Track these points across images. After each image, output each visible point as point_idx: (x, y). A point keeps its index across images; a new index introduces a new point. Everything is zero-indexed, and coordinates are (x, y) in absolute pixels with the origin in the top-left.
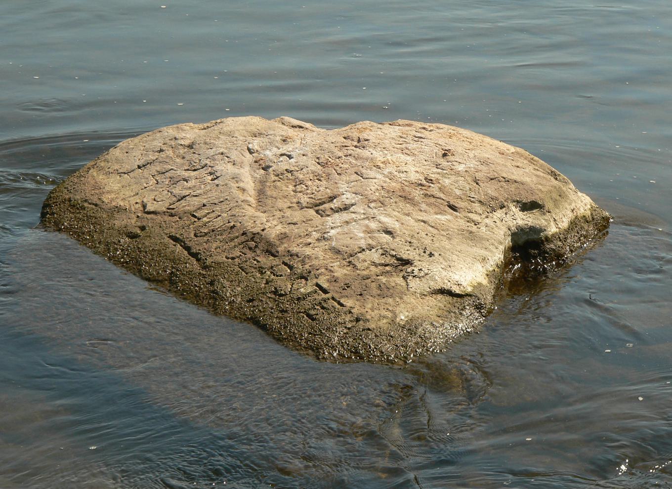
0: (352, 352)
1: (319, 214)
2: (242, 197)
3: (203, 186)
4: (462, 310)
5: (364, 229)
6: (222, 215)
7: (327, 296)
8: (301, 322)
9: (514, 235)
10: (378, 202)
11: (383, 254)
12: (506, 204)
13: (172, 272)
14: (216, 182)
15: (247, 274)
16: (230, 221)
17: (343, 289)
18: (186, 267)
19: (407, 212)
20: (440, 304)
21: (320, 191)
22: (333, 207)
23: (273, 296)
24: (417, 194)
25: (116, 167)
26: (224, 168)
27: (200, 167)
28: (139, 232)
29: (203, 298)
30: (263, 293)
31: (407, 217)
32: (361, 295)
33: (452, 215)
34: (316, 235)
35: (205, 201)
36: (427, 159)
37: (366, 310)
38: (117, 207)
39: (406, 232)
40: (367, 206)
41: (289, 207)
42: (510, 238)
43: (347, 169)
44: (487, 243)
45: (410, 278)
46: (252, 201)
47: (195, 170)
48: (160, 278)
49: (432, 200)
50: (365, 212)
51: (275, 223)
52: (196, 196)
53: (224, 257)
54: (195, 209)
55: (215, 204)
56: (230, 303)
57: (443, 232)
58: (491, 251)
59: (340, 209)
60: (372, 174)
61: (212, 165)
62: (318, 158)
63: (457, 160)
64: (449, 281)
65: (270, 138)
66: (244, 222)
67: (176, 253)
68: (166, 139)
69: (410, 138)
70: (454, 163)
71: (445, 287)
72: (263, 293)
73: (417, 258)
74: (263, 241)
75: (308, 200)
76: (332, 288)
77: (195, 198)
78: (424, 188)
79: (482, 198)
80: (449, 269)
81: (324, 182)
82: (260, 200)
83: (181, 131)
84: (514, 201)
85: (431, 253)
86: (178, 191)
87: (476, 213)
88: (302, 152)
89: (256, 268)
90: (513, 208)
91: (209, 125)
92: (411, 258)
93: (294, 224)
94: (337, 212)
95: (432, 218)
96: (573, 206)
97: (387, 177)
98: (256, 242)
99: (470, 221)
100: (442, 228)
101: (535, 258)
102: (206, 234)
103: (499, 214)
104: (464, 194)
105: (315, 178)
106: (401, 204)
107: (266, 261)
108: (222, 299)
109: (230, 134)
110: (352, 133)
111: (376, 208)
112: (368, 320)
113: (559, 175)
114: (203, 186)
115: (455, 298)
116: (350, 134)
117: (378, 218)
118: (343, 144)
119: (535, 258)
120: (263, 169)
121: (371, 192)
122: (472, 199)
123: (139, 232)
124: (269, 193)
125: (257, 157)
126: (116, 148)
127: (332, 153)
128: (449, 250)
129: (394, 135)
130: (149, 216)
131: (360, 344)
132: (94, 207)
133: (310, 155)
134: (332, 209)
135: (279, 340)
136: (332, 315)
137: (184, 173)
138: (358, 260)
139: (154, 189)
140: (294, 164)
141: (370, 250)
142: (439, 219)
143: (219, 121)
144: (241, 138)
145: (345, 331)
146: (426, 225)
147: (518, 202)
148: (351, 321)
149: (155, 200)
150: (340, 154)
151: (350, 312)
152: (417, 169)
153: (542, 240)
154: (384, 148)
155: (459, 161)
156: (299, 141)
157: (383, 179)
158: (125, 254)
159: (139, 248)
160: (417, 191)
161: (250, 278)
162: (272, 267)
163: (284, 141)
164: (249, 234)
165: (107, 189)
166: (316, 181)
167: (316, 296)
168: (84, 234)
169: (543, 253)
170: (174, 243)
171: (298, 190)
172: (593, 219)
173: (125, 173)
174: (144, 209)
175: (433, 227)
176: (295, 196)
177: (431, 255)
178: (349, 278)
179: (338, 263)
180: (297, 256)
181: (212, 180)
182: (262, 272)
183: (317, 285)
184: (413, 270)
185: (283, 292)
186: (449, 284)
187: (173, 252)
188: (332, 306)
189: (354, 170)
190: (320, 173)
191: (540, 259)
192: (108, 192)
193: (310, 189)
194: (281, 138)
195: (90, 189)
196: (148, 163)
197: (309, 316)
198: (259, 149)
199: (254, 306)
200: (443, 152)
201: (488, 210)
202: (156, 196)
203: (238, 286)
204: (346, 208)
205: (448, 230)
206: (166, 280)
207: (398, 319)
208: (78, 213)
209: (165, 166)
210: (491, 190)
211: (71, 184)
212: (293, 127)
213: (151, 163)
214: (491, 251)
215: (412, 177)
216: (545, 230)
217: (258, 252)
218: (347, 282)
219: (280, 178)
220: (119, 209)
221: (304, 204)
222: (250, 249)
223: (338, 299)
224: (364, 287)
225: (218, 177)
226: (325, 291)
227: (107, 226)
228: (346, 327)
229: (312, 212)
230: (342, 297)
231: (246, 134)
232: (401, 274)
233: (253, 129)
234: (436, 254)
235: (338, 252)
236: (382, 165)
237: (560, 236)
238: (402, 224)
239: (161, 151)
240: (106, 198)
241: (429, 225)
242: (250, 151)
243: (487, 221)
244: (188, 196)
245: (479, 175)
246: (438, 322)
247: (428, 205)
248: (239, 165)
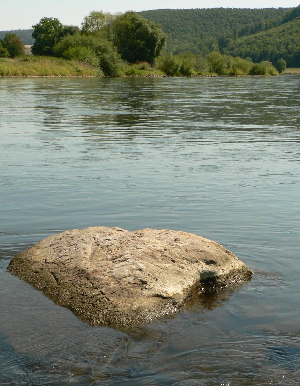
0: (107, 321)
4: (166, 304)
5: (129, 268)
7: (104, 296)
11: (135, 279)
12: (199, 261)
20: (156, 302)
24: (158, 255)
26: (82, 245)
30: (78, 295)
33: (172, 264)
34: (108, 271)
36: (167, 241)
42: (199, 276)
44: (186, 276)
46: (88, 257)
49: (165, 257)
57: (166, 271)
58: (187, 280)
60: (141, 247)
62: (120, 241)
72: (78, 295)
74: (86, 273)
76: (107, 293)
77: (66, 257)
79: (188, 258)
81: (120, 250)
84: (203, 260)
85: (157, 279)
86: (60, 254)
87: (184, 264)
88: (115, 238)
89: (79, 284)
90: (202, 263)
93: (101, 266)
94: (122, 262)
95: (163, 265)
96: (233, 264)
97: (147, 248)
99: (180, 267)
101: (212, 286)
102: (64, 271)
103: (195, 265)
107: (83, 281)
112: (119, 307)
113: (230, 253)
128: (166, 278)
133: (117, 239)
134: (119, 260)
135: (77, 315)
145: (107, 312)
147: (205, 260)
150: (130, 239)
151: (112, 303)
152: (161, 245)
162: (85, 284)
169: (215, 284)
172: (243, 271)
177: (157, 280)
178: (116, 288)
180: (97, 279)
183: (101, 292)
185: (86, 295)
186: (162, 292)
190: (119, 246)
192: (35, 255)
197: (93, 305)
198: (98, 238)
203: (69, 292)
205: (168, 270)
210: (193, 254)
212: (117, 230)
214: (187, 280)
220: (36, 262)
224: (121, 293)
226: (103, 294)
228: (107, 310)
229: (111, 262)
232: (141, 288)
234: (159, 280)
236: (146, 243)
237: (225, 277)
242: (94, 238)
243: (189, 267)
245: (188, 249)
246: (152, 309)
247: (163, 259)
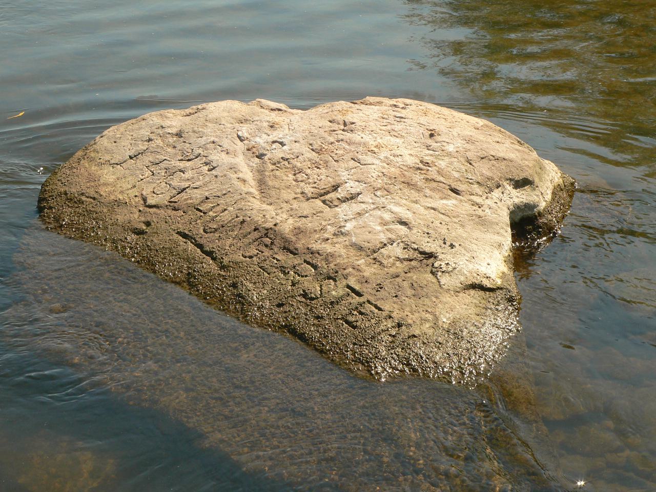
1: (327, 205)
2: (245, 189)
3: (201, 177)
5: (379, 221)
6: (228, 208)
8: (342, 331)
9: (512, 214)
10: (383, 189)
11: (404, 248)
13: (189, 274)
14: (214, 172)
15: (269, 274)
16: (239, 215)
17: (377, 291)
18: (203, 267)
19: (415, 199)
20: (475, 301)
21: (321, 179)
22: (339, 197)
23: (303, 300)
24: (417, 178)
25: (107, 157)
26: (216, 157)
27: (194, 157)
28: (144, 228)
29: (229, 302)
31: (416, 205)
32: (396, 296)
35: (207, 194)
36: (416, 140)
37: (406, 313)
38: (116, 201)
39: (420, 222)
40: (373, 195)
41: (295, 198)
43: (343, 156)
45: (440, 274)
46: (254, 191)
47: (189, 160)
48: (178, 280)
49: (434, 185)
50: (373, 201)
51: (285, 216)
52: (196, 188)
53: (241, 255)
54: (198, 202)
55: (219, 197)
56: (259, 308)
57: (454, 220)
59: (347, 198)
61: (206, 155)
62: (311, 144)
63: (444, 140)
64: (478, 275)
65: (256, 125)
66: (254, 217)
67: (189, 251)
68: (153, 128)
69: (392, 118)
70: (445, 144)
71: (476, 281)
73: (439, 250)
74: (278, 237)
75: (312, 190)
77: (195, 191)
78: (423, 172)
79: (479, 179)
80: (473, 260)
81: (323, 169)
82: (262, 191)
83: (165, 119)
84: (507, 180)
87: (477, 195)
88: (293, 139)
89: (277, 268)
91: (191, 111)
92: (433, 250)
93: (305, 217)
95: (440, 204)
97: (384, 162)
98: (270, 238)
100: (453, 215)
102: (216, 230)
103: (496, 193)
104: (462, 176)
105: (313, 166)
106: (406, 191)
108: (250, 304)
109: (217, 121)
110: (336, 116)
111: (383, 197)
114: (201, 177)
115: (488, 293)
116: (334, 117)
117: (388, 207)
118: (332, 129)
119: (530, 233)
120: (257, 157)
121: (373, 179)
122: (471, 181)
123: (144, 228)
124: (270, 183)
125: (248, 145)
126: (102, 137)
127: (324, 138)
128: (466, 239)
129: (376, 116)
130: (153, 210)
131: (410, 354)
132: (92, 200)
136: (373, 321)
137: (178, 163)
138: (383, 256)
139: (151, 181)
140: (289, 152)
141: (392, 244)
142: (446, 204)
143: (200, 107)
144: (229, 125)
146: (437, 212)
147: (511, 180)
148: (393, 327)
149: (154, 192)
150: (332, 139)
151: (390, 317)
153: (536, 216)
154: (372, 131)
155: (447, 140)
156: (286, 127)
157: (381, 164)
158: (135, 253)
159: (148, 246)
160: (417, 176)
161: (274, 279)
162: (294, 267)
163: (272, 127)
164: (261, 229)
165: (102, 181)
166: (315, 169)
167: (350, 300)
168: (87, 230)
169: (537, 228)
170: (184, 240)
171: (300, 179)
173: (117, 164)
174: (145, 203)
175: (444, 214)
176: (298, 186)
179: (363, 260)
180: (319, 253)
181: (209, 170)
182: (284, 272)
183: (348, 287)
184: (441, 265)
185: (313, 296)
186: (479, 277)
187: (185, 250)
188: (370, 311)
189: (351, 155)
191: (535, 234)
193: (311, 178)
194: (267, 123)
195: (84, 181)
196: (139, 153)
197: (347, 322)
198: (249, 136)
199: (285, 312)
200: (430, 133)
201: (487, 191)
202: (154, 188)
204: (352, 197)
205: (458, 216)
206: (184, 282)
207: (440, 322)
208: (77, 207)
209: (158, 157)
210: (484, 169)
211: (64, 176)
212: (272, 110)
213: (142, 153)
215: (408, 161)
216: (538, 205)
217: (276, 249)
218: (379, 282)
219: (278, 167)
220: (118, 203)
221: (310, 195)
222: (266, 246)
223: (374, 303)
225: (214, 168)
226: (359, 294)
227: (110, 222)
228: (390, 335)
229: (318, 203)
230: (378, 299)
231: (232, 121)
233: (237, 114)
235: (360, 248)
236: (376, 150)
238: (414, 213)
239: (150, 140)
240: (103, 191)
241: (439, 212)
242: (241, 139)
243: (488, 202)
244: (187, 188)
245: (470, 155)
248: (226, 154)
